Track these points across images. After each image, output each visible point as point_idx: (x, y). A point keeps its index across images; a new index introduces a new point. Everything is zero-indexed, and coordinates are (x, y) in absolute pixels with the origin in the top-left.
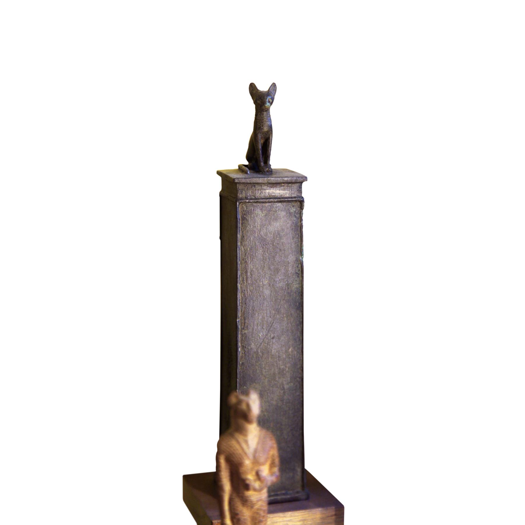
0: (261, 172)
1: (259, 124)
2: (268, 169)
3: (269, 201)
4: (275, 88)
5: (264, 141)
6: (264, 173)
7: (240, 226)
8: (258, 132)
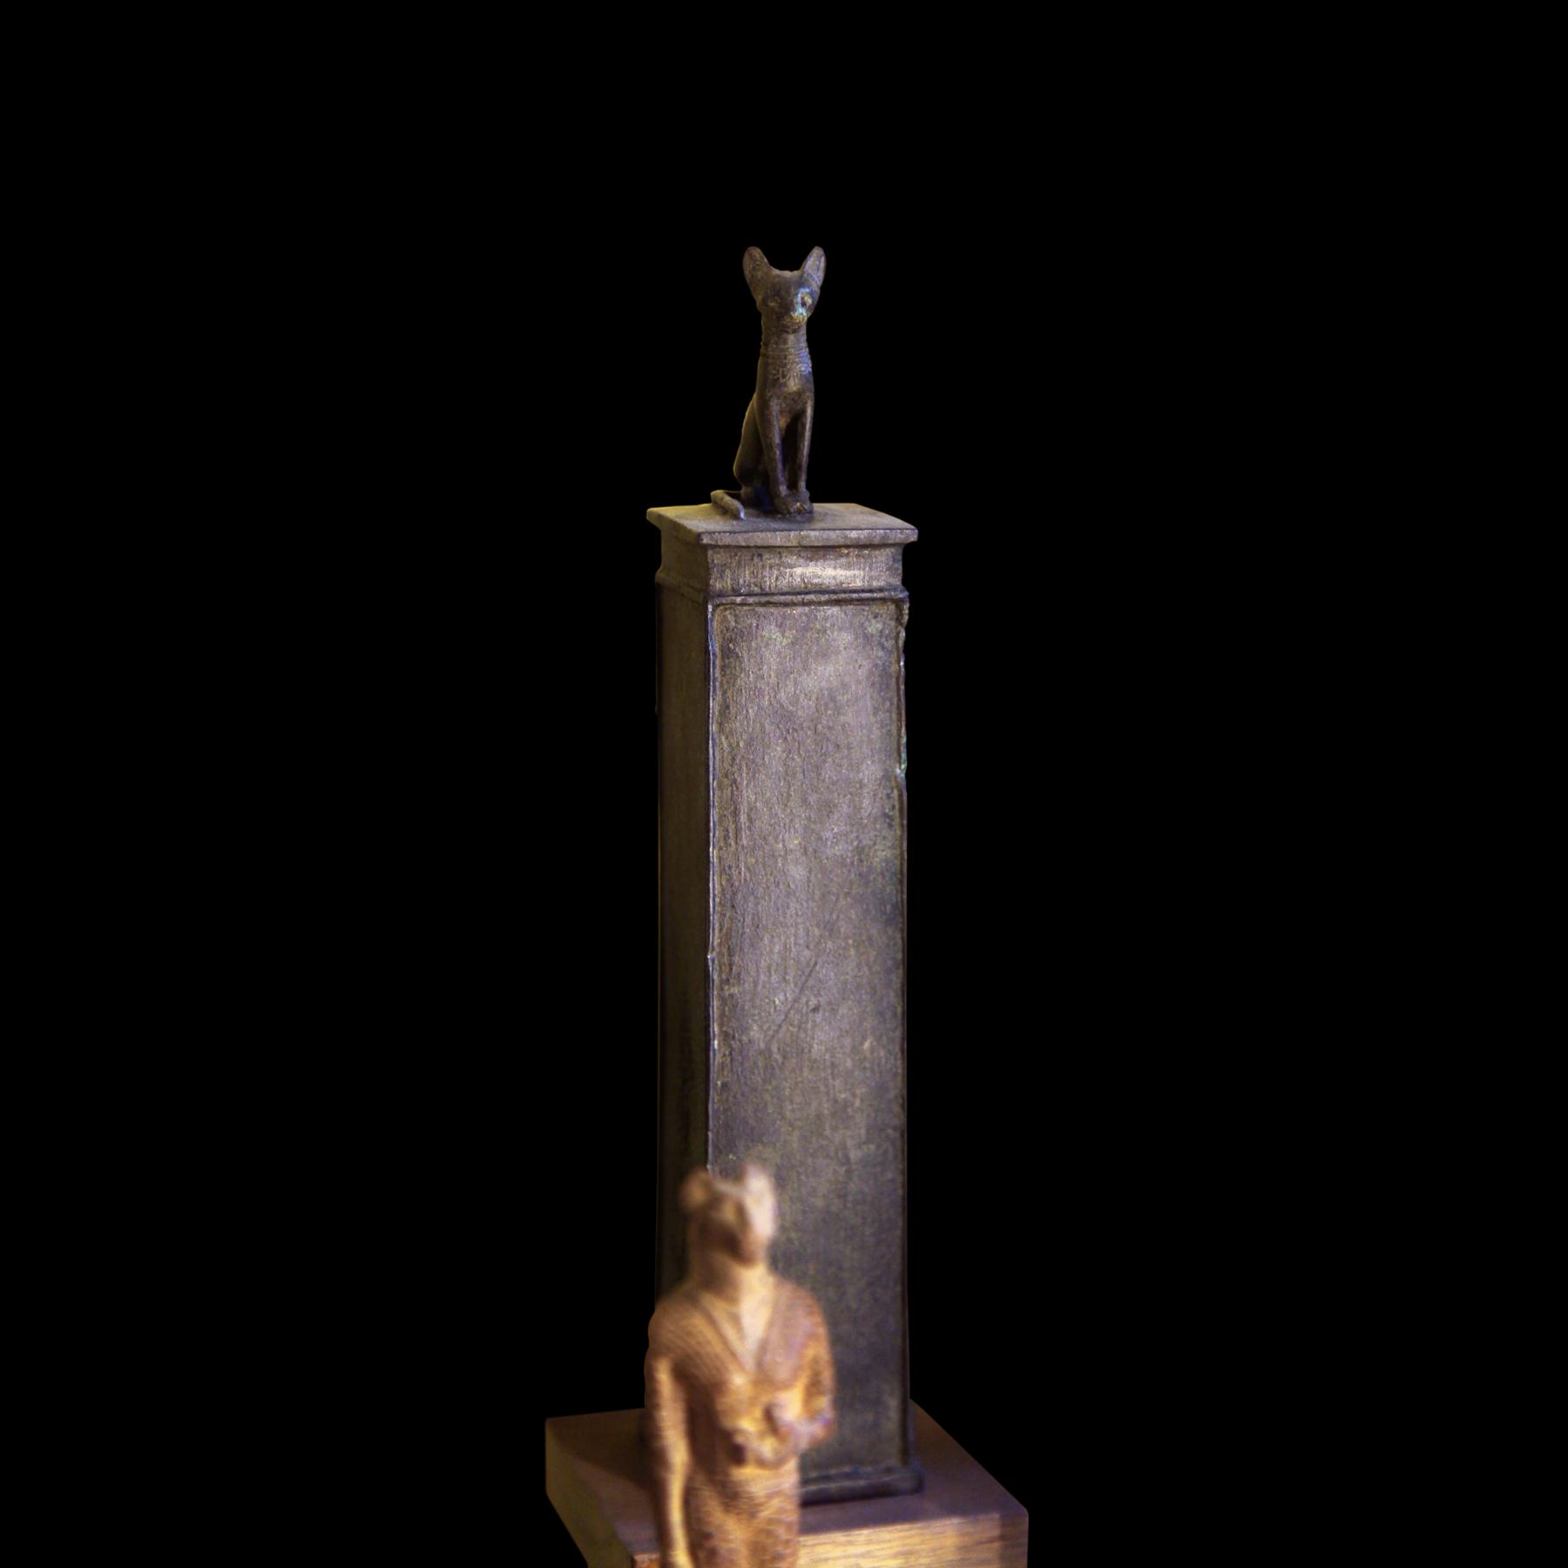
0: (778, 512)
1: (775, 369)
2: (801, 506)
3: (803, 599)
4: (820, 262)
5: (789, 420)
6: (788, 516)
7: (717, 675)
8: (769, 394)
